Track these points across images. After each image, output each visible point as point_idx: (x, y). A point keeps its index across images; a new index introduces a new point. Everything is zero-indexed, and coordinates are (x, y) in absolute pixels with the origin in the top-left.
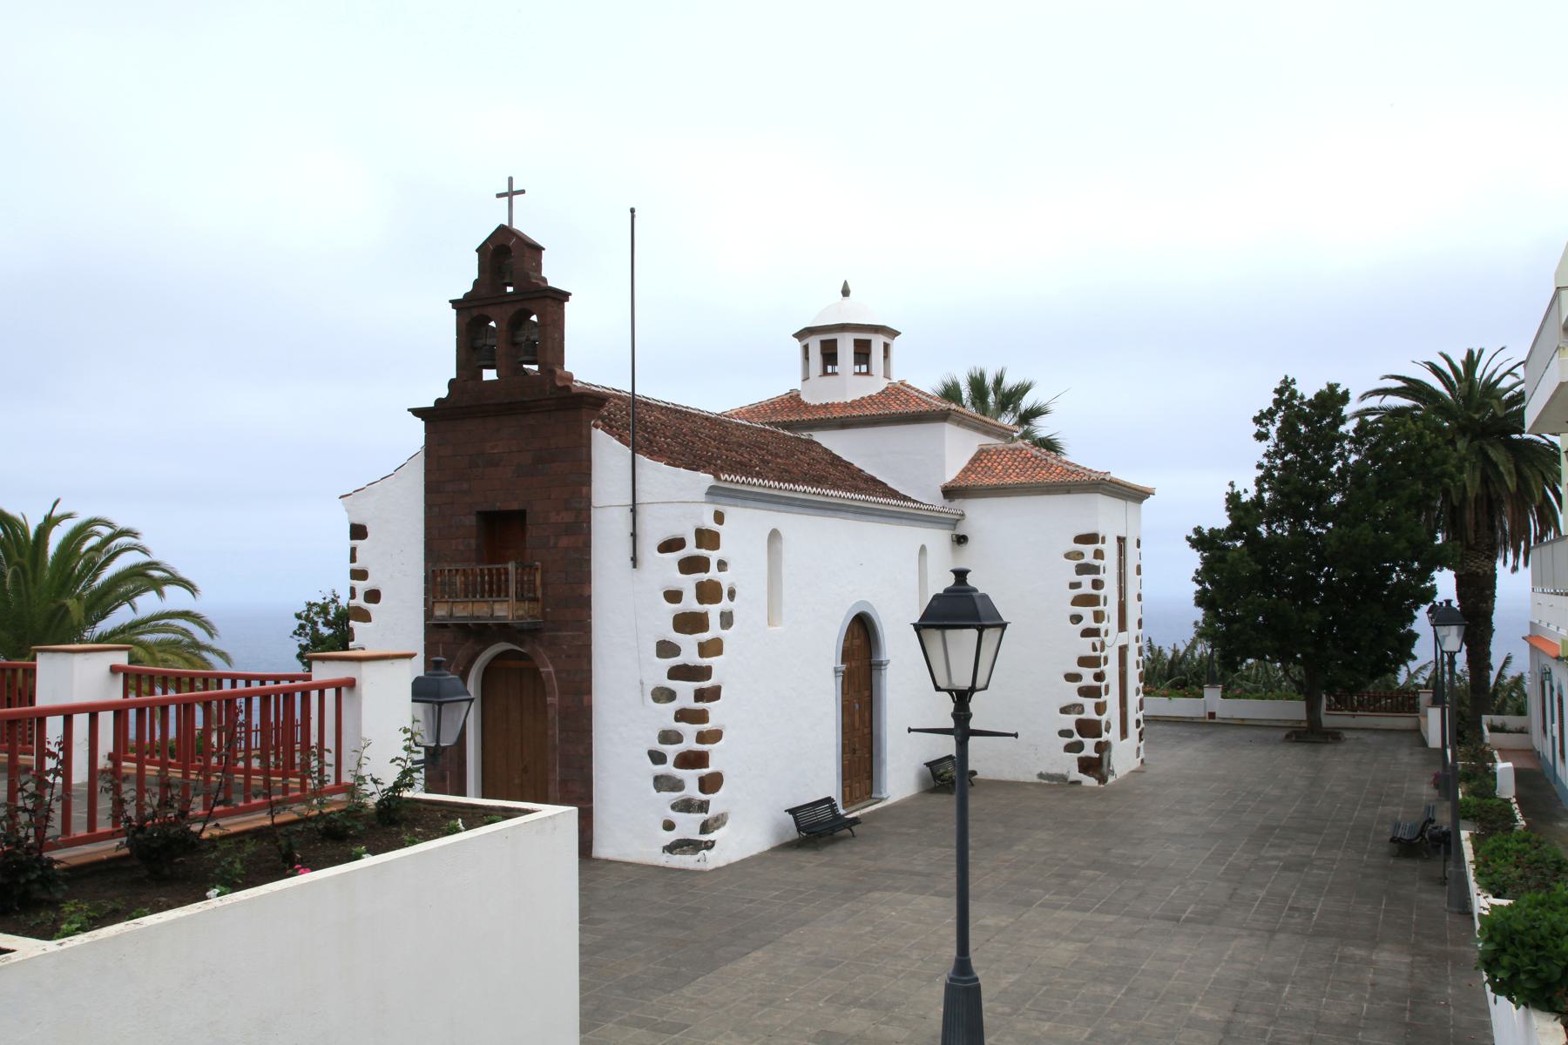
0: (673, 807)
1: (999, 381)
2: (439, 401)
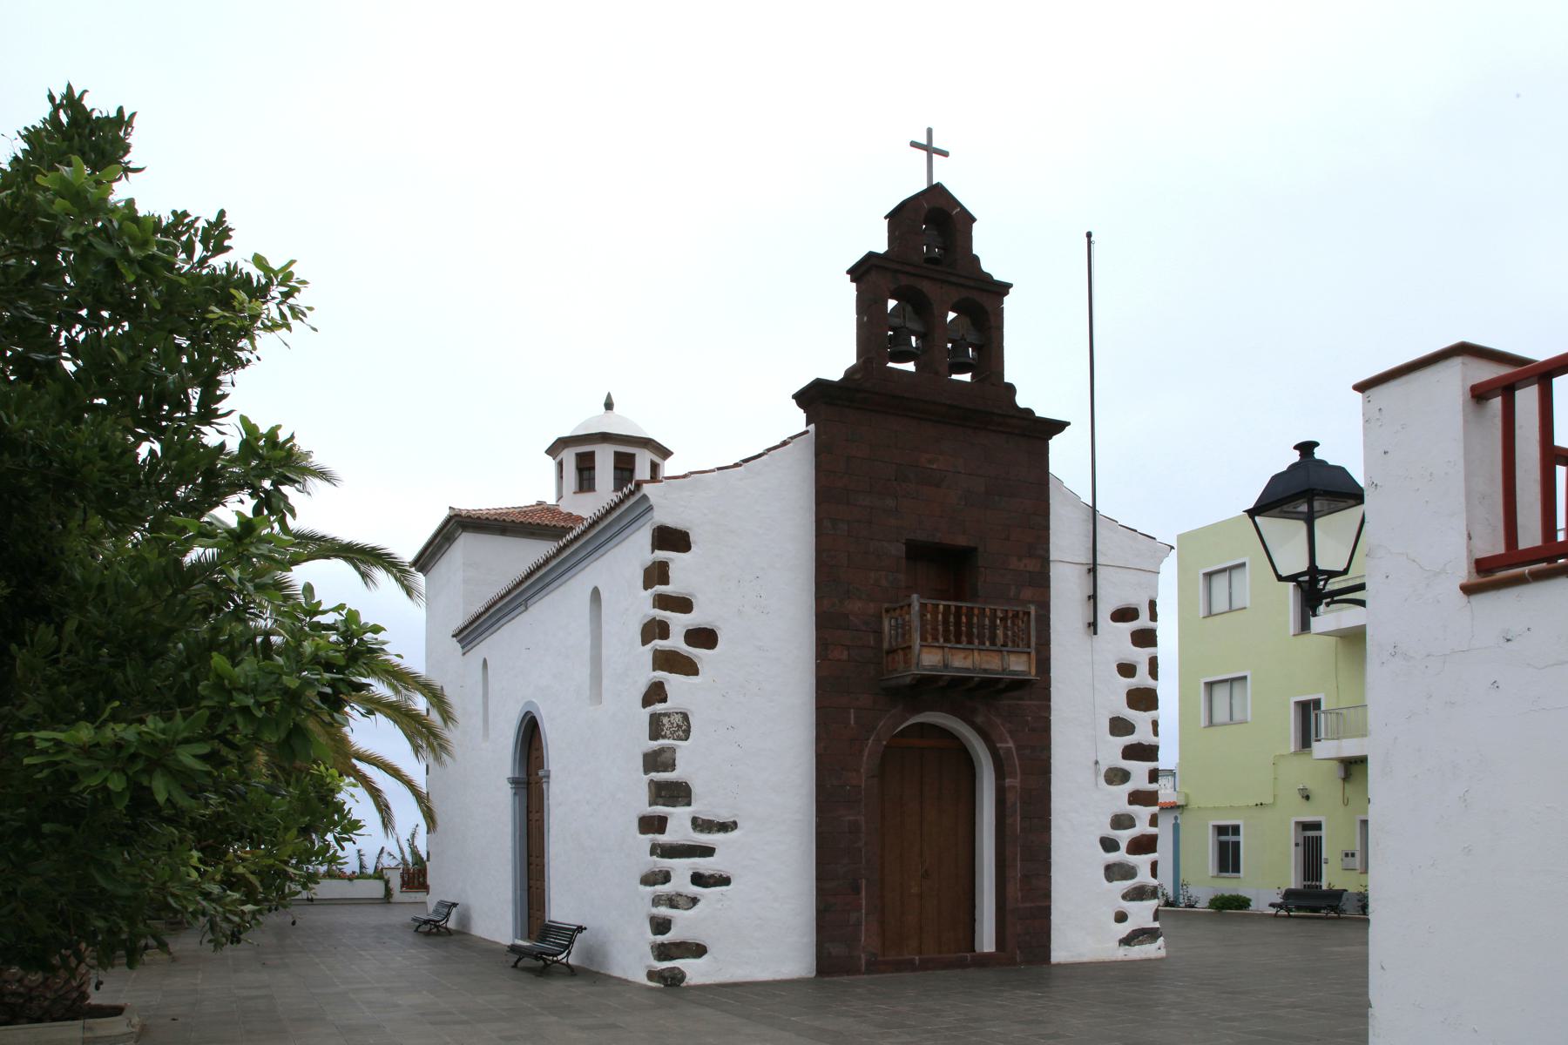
0: (1124, 897)
2: (1011, 389)
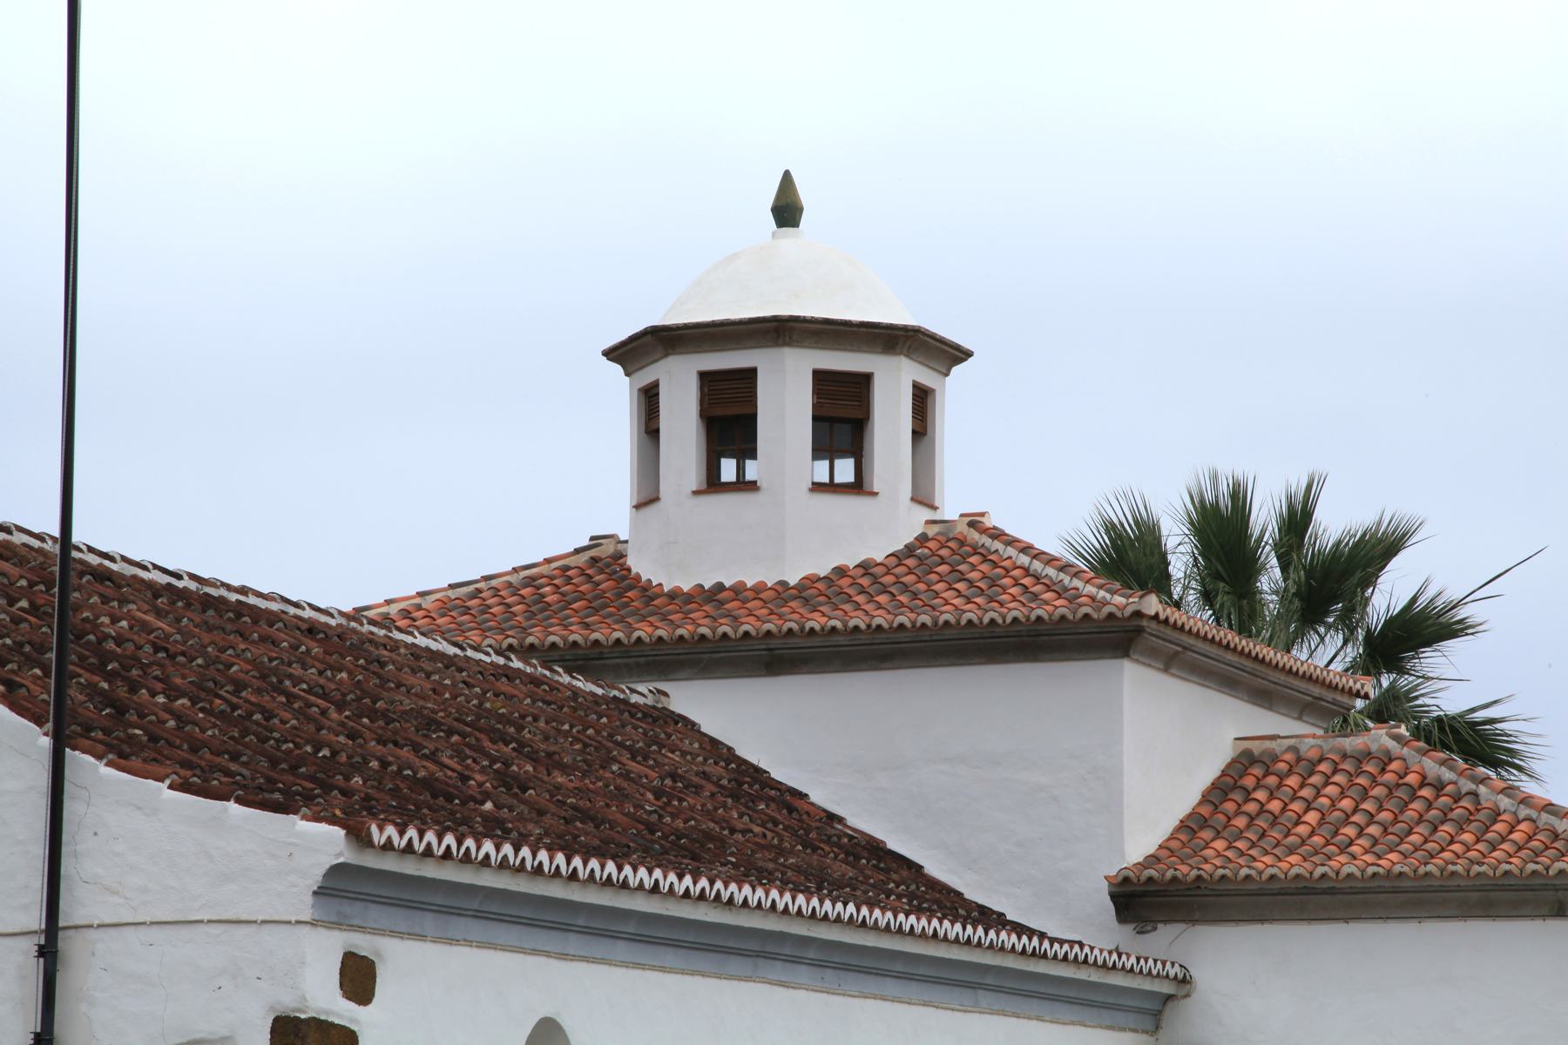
1: (1297, 519)
